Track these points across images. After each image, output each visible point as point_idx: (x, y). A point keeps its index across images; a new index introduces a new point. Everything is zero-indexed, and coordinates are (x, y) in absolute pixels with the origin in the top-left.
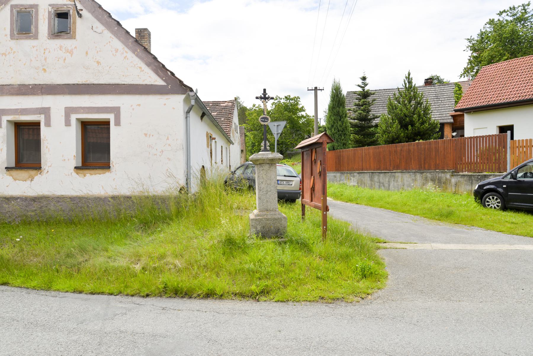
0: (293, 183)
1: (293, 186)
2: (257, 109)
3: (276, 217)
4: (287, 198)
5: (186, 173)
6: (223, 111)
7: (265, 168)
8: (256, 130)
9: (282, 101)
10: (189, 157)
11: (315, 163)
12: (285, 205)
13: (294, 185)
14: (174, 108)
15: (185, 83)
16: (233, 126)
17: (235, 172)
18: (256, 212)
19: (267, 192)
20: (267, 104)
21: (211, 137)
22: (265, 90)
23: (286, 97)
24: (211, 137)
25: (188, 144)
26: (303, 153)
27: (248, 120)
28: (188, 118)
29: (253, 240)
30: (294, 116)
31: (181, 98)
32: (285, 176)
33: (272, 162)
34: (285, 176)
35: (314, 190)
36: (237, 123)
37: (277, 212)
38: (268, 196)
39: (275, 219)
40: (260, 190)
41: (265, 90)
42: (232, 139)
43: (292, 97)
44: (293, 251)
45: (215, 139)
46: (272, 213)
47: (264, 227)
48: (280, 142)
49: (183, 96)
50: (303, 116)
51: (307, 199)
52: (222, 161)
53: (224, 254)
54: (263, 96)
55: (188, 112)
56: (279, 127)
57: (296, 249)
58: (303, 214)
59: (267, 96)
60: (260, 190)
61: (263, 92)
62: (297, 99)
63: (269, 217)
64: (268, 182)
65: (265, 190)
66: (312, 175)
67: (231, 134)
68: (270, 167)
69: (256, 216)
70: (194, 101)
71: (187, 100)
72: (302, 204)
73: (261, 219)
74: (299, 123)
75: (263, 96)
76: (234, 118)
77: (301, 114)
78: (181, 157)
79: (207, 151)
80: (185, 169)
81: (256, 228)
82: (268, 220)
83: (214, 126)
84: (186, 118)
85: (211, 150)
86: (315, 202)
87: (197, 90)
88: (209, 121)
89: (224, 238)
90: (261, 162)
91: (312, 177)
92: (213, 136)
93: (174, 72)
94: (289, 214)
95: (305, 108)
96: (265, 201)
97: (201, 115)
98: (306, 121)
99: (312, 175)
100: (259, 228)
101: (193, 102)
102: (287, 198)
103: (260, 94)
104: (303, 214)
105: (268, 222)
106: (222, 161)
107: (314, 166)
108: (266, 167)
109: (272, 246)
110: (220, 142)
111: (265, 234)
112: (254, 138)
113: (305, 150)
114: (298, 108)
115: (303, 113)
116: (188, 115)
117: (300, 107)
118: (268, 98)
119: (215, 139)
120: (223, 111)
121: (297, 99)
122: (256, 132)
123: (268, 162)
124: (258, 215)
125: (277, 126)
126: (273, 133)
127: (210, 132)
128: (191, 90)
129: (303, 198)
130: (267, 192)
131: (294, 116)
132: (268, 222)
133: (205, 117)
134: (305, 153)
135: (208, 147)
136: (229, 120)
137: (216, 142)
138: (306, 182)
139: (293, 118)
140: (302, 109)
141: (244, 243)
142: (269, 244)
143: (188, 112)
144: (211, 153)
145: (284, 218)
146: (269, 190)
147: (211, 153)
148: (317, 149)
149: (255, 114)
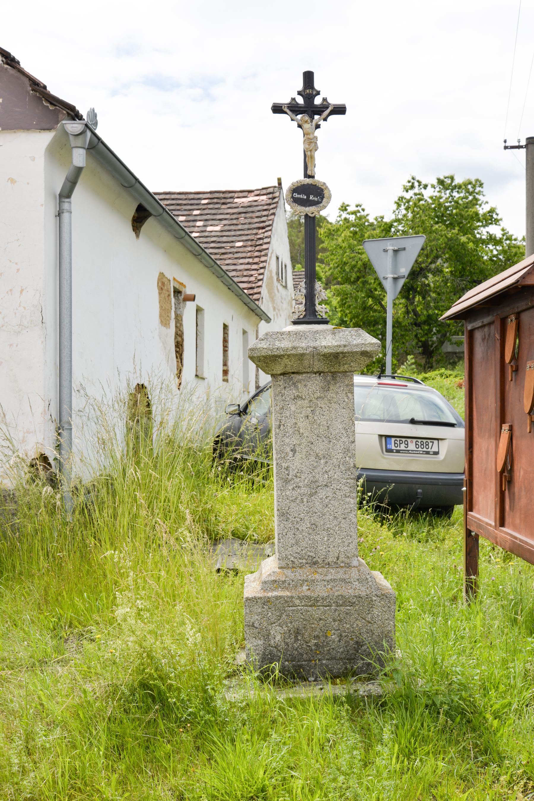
0: (444, 448)
1: (442, 456)
2: (352, 218)
3: (348, 591)
4: (410, 500)
5: (54, 410)
6: (242, 220)
7: (303, 391)
8: (347, 280)
9: (428, 193)
10: (65, 352)
11: (516, 370)
12: (409, 527)
13: (446, 454)
14: (12, 181)
15: (54, 90)
16: (272, 265)
17: (246, 407)
18: (270, 566)
19: (314, 487)
20: (317, 133)
21: (177, 292)
22: (308, 77)
23: (441, 182)
24: (177, 292)
25: (65, 305)
26: (471, 334)
27: (324, 250)
28: (65, 215)
29: (244, 693)
30: (463, 239)
31: (36, 144)
32: (413, 422)
33: (335, 367)
34: (413, 422)
35: (510, 481)
36: (286, 259)
37: (354, 574)
38: (318, 506)
39: (345, 601)
40: (287, 481)
41: (308, 77)
42: (265, 306)
43: (458, 180)
44: (408, 754)
45: (192, 298)
46: (333, 574)
47: (297, 632)
48: (423, 318)
49: (45, 139)
50: (492, 239)
51: (485, 513)
52: (225, 372)
53: (118, 749)
54: (300, 100)
55: (66, 194)
56: (402, 254)
57: (425, 740)
58: (472, 565)
59: (318, 101)
60: (287, 481)
61: (300, 86)
62: (473, 187)
63: (321, 591)
64: (320, 447)
65: (306, 478)
66: (503, 421)
67: (264, 291)
68: (326, 389)
69: (267, 585)
70: (82, 152)
71: (59, 150)
72: (468, 533)
73: (288, 601)
74: (480, 258)
75: (300, 100)
76: (274, 241)
77: (483, 232)
78: (37, 353)
79: (161, 341)
80: (52, 394)
81: (267, 636)
82: (314, 602)
83: (190, 257)
84: (59, 214)
85: (179, 335)
86: (515, 528)
87: (93, 115)
88: (167, 238)
89: (125, 678)
90: (290, 365)
91: (506, 427)
92: (189, 291)
93: (14, 53)
94: (413, 564)
95: (501, 213)
96: (305, 526)
97: (132, 212)
98: (504, 252)
99: (503, 421)
100: (277, 636)
101: (79, 157)
102: (410, 500)
103: (290, 91)
104: (472, 565)
105: (316, 612)
106: (225, 372)
107: (510, 386)
108: (312, 386)
109: (318, 721)
110: (215, 309)
111: (292, 667)
112: (342, 304)
113: (478, 324)
114: (477, 214)
115: (495, 230)
116: (66, 206)
117: (482, 210)
118: (319, 110)
119: (192, 298)
120: (242, 220)
121: (473, 187)
122: (347, 287)
123: (318, 366)
124: (275, 584)
125: (396, 251)
126: (381, 275)
127: (177, 274)
128: (73, 114)
129: (470, 507)
130: (314, 487)
131: (463, 239)
132: (316, 612)
133: (150, 224)
134: (478, 336)
135: (164, 321)
136: (259, 247)
137: (199, 310)
138: (482, 444)
139: (463, 245)
140: (490, 218)
141: (207, 702)
142: (316, 708)
143: (66, 194)
144: (179, 346)
145: (384, 596)
146: (322, 479)
147: (179, 346)
148: (526, 317)
149: (347, 233)
